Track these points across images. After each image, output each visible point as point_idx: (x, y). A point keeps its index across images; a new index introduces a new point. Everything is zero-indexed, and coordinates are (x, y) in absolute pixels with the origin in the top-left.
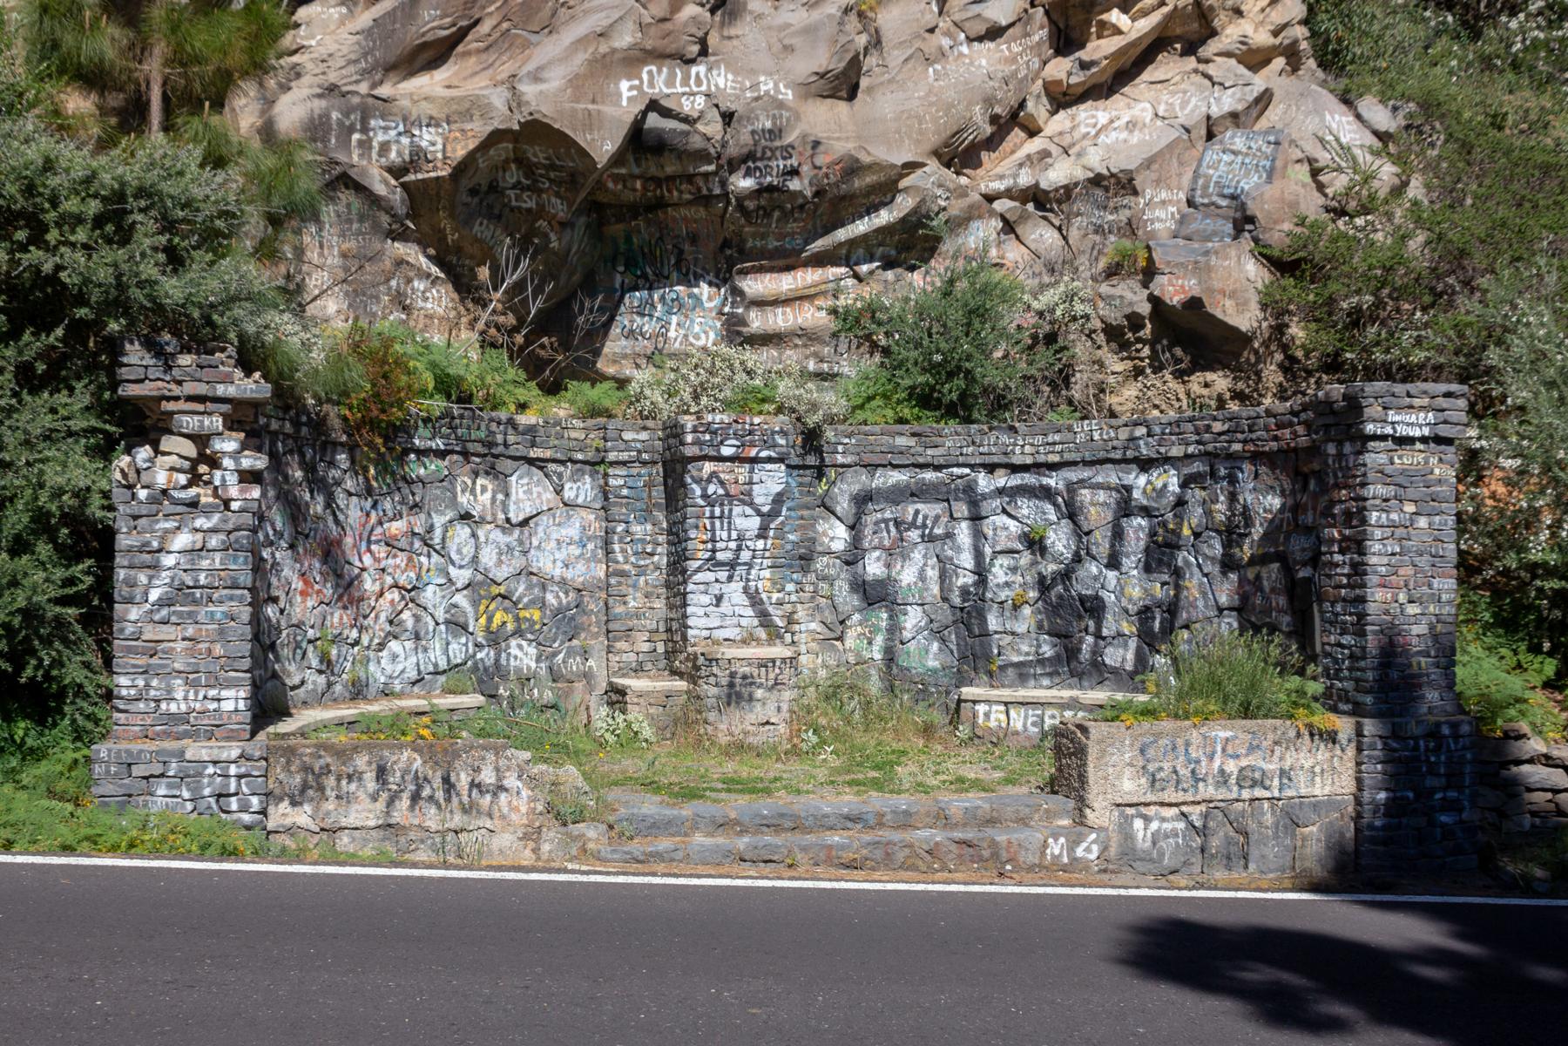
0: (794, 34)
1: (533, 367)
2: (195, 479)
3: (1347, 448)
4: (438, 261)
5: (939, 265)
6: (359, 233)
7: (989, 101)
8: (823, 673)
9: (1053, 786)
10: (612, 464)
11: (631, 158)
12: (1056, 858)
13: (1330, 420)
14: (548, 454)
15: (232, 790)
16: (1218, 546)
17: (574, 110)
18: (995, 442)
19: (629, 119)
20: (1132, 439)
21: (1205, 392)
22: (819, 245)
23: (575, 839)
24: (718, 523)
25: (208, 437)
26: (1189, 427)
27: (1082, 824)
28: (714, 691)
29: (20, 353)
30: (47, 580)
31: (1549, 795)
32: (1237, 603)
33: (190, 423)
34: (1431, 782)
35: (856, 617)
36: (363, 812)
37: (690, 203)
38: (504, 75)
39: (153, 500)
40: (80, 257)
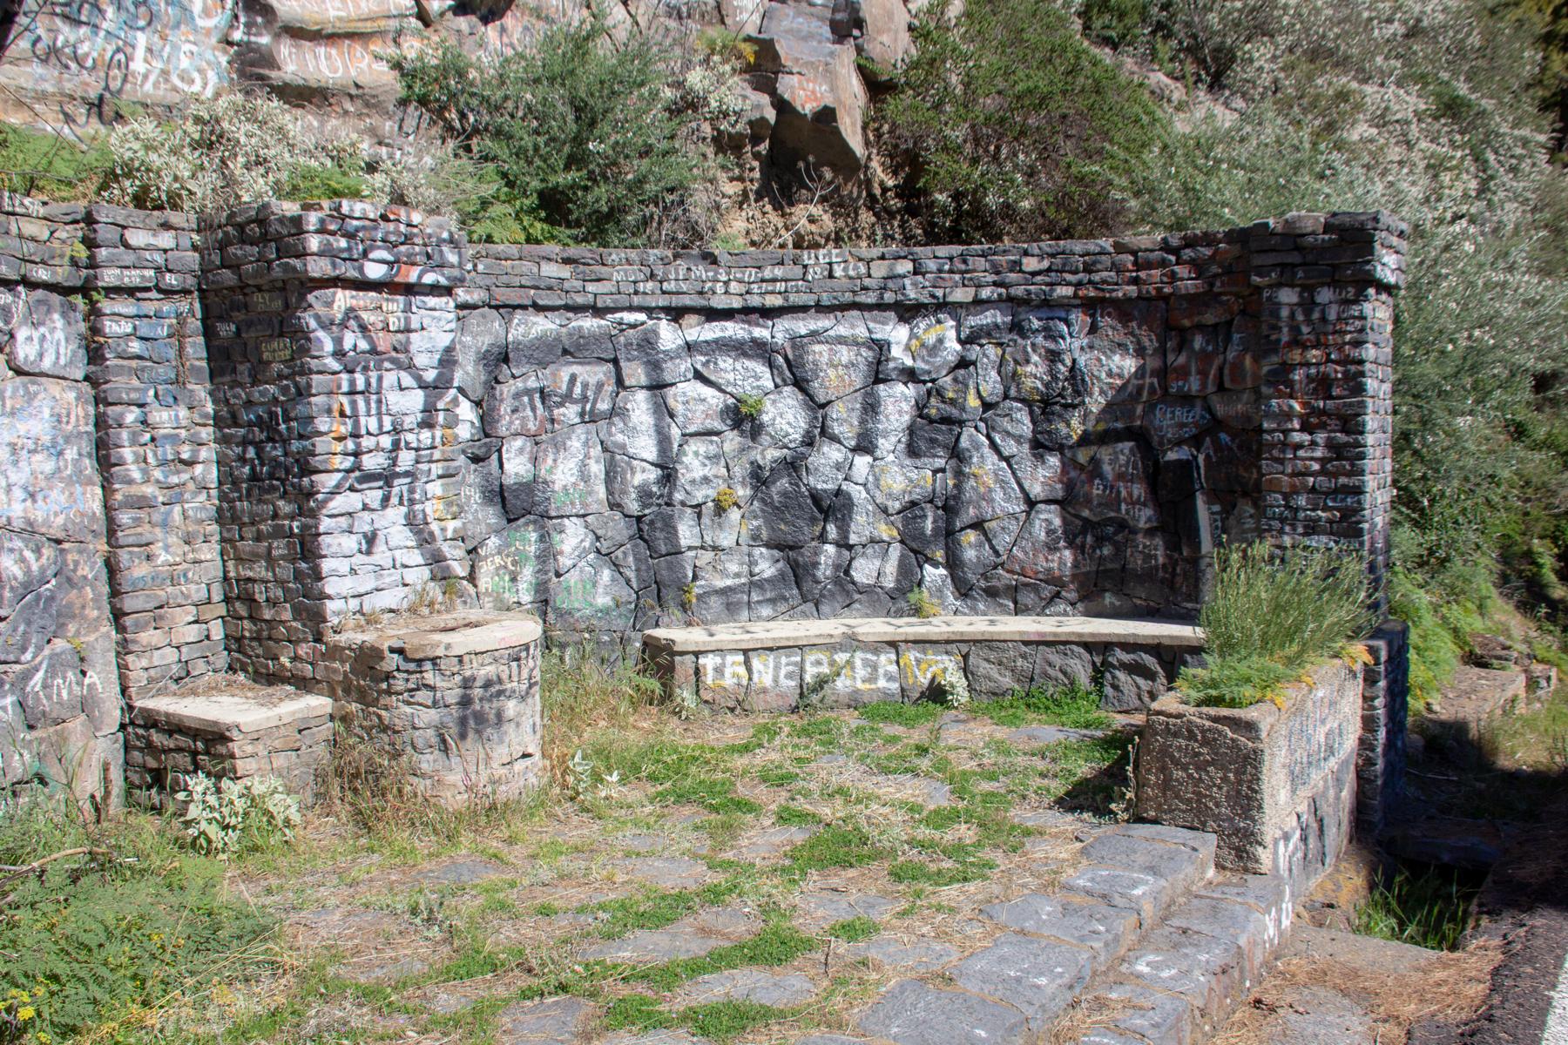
10: (112, 291)
16: (1027, 420)
24: (360, 400)
28: (429, 716)
32: (1059, 493)
35: (493, 542)
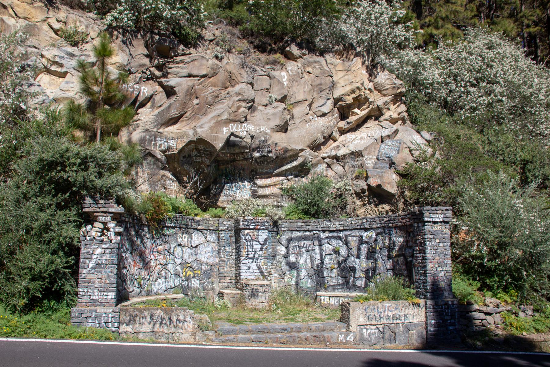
0: (270, 115)
1: (199, 204)
2: (103, 234)
3: (420, 225)
4: (173, 174)
5: (310, 176)
7: (323, 133)
8: (279, 288)
9: (341, 320)
10: (220, 230)
11: (226, 148)
12: (341, 340)
13: (415, 217)
14: (203, 228)
15: (110, 321)
16: (386, 252)
17: (211, 136)
18: (325, 224)
19: (226, 138)
20: (362, 223)
21: (383, 210)
22: (277, 171)
23: (205, 335)
25: (107, 223)
26: (378, 219)
27: (349, 331)
28: (247, 293)
29: (57, 200)
30: (61, 262)
31: (480, 321)
33: (102, 219)
34: (446, 317)
35: (288, 273)
36: (146, 328)
37: (242, 160)
38: (193, 126)
39: (91, 240)
40: (74, 174)
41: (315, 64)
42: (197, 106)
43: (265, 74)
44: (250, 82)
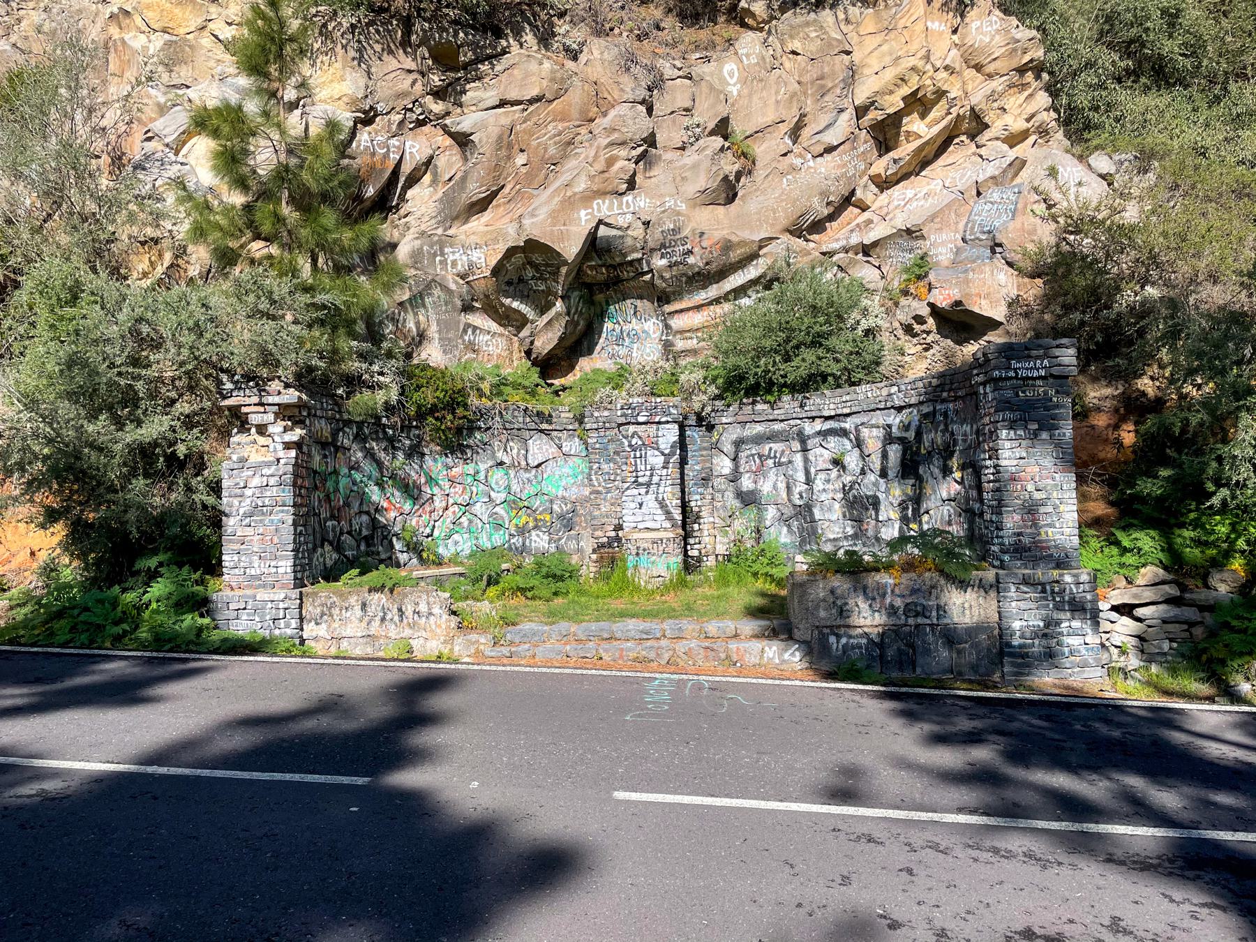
6: (446, 311)
7: (824, 194)
12: (769, 659)
20: (890, 395)
41: (807, 30)
42: (524, 170)
43: (681, 73)
44: (640, 99)
